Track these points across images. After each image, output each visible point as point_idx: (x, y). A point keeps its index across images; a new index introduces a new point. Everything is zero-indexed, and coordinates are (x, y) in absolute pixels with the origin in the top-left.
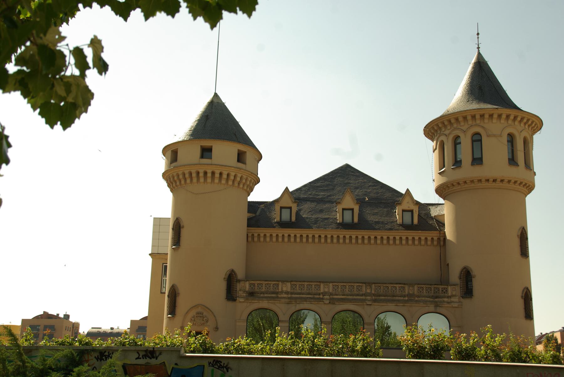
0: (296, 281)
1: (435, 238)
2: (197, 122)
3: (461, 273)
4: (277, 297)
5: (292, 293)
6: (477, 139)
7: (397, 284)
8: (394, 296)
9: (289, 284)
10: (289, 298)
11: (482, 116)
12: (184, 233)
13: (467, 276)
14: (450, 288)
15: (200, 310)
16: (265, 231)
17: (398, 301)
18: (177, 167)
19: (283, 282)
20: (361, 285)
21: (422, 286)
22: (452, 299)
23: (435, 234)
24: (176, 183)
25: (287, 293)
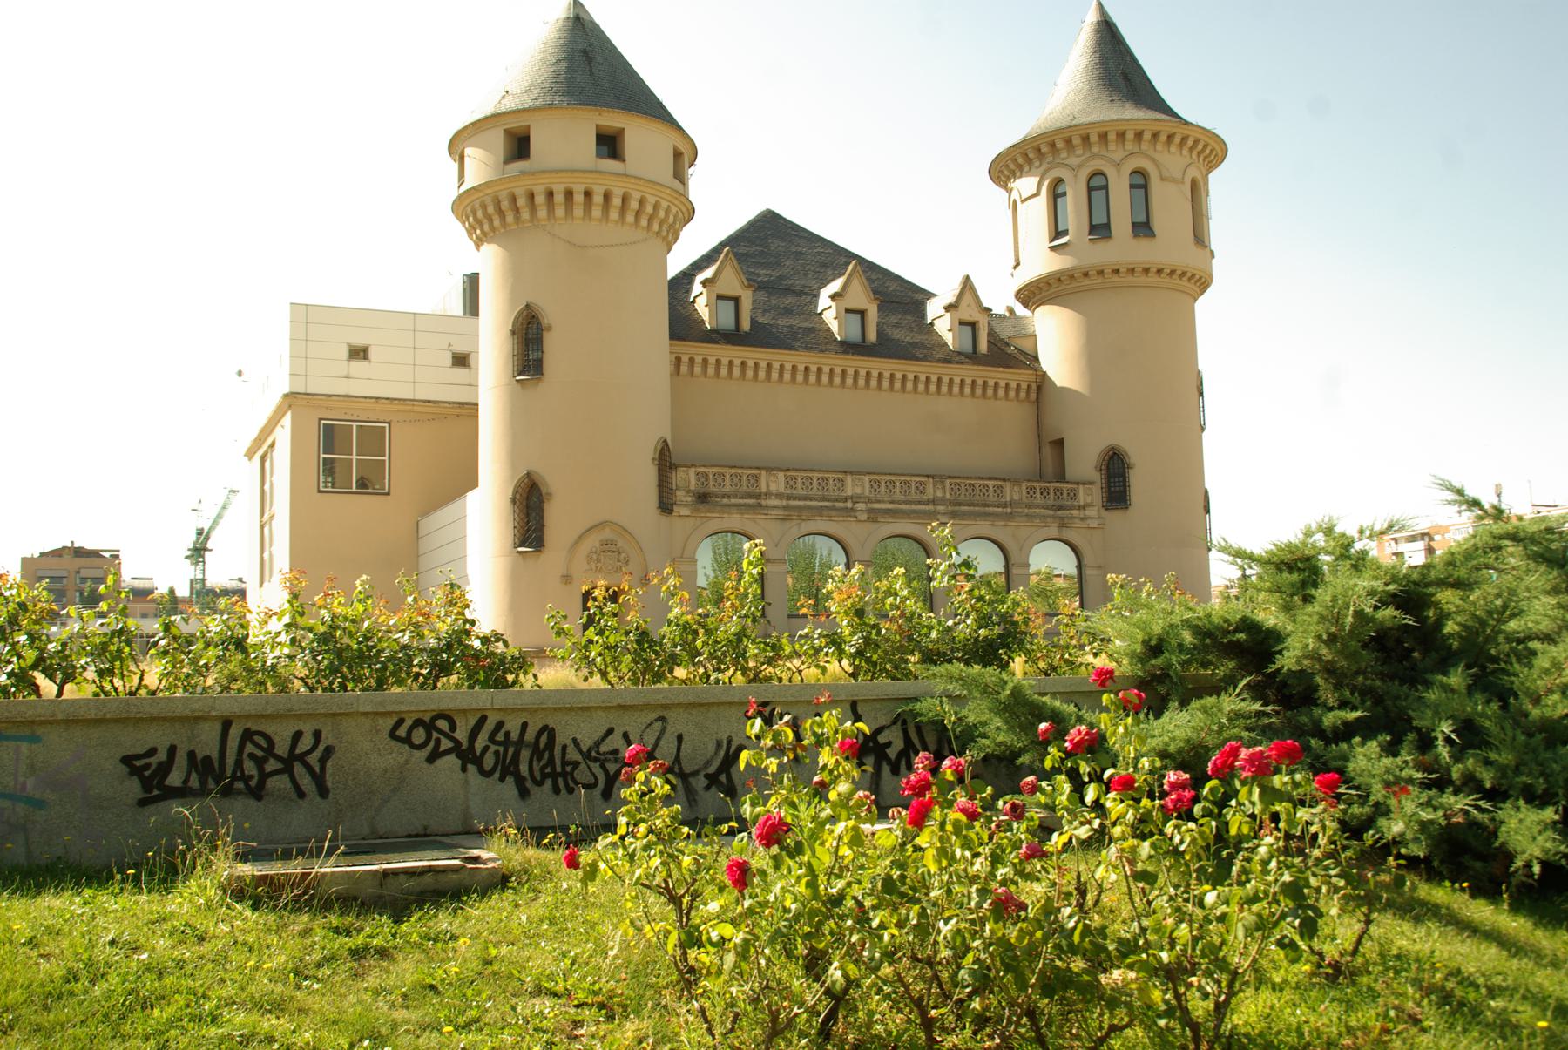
2: (564, 65)
6: (1141, 183)
8: (985, 505)
9: (781, 475)
10: (786, 508)
11: (1103, 137)
12: (554, 348)
13: (1115, 469)
15: (607, 534)
16: (692, 350)
17: (996, 515)
18: (533, 173)
19: (770, 470)
23: (1020, 377)
24: (491, 220)
25: (779, 496)
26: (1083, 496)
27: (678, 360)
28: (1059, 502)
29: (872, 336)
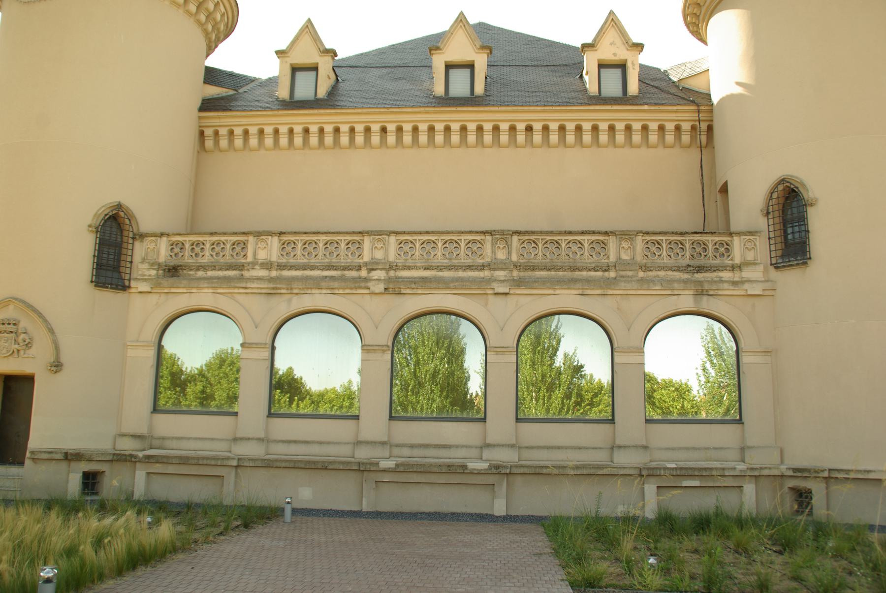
0: (295, 233)
1: (686, 126)
3: (771, 198)
4: (241, 278)
5: (281, 267)
7: (583, 233)
8: (574, 268)
9: (274, 243)
10: (271, 280)
13: (790, 206)
14: (737, 242)
16: (244, 121)
17: (588, 281)
19: (258, 234)
20: (478, 237)
21: (658, 238)
22: (746, 274)
25: (268, 265)
26: (738, 250)
27: (202, 133)
28: (702, 261)
29: (479, 89)
